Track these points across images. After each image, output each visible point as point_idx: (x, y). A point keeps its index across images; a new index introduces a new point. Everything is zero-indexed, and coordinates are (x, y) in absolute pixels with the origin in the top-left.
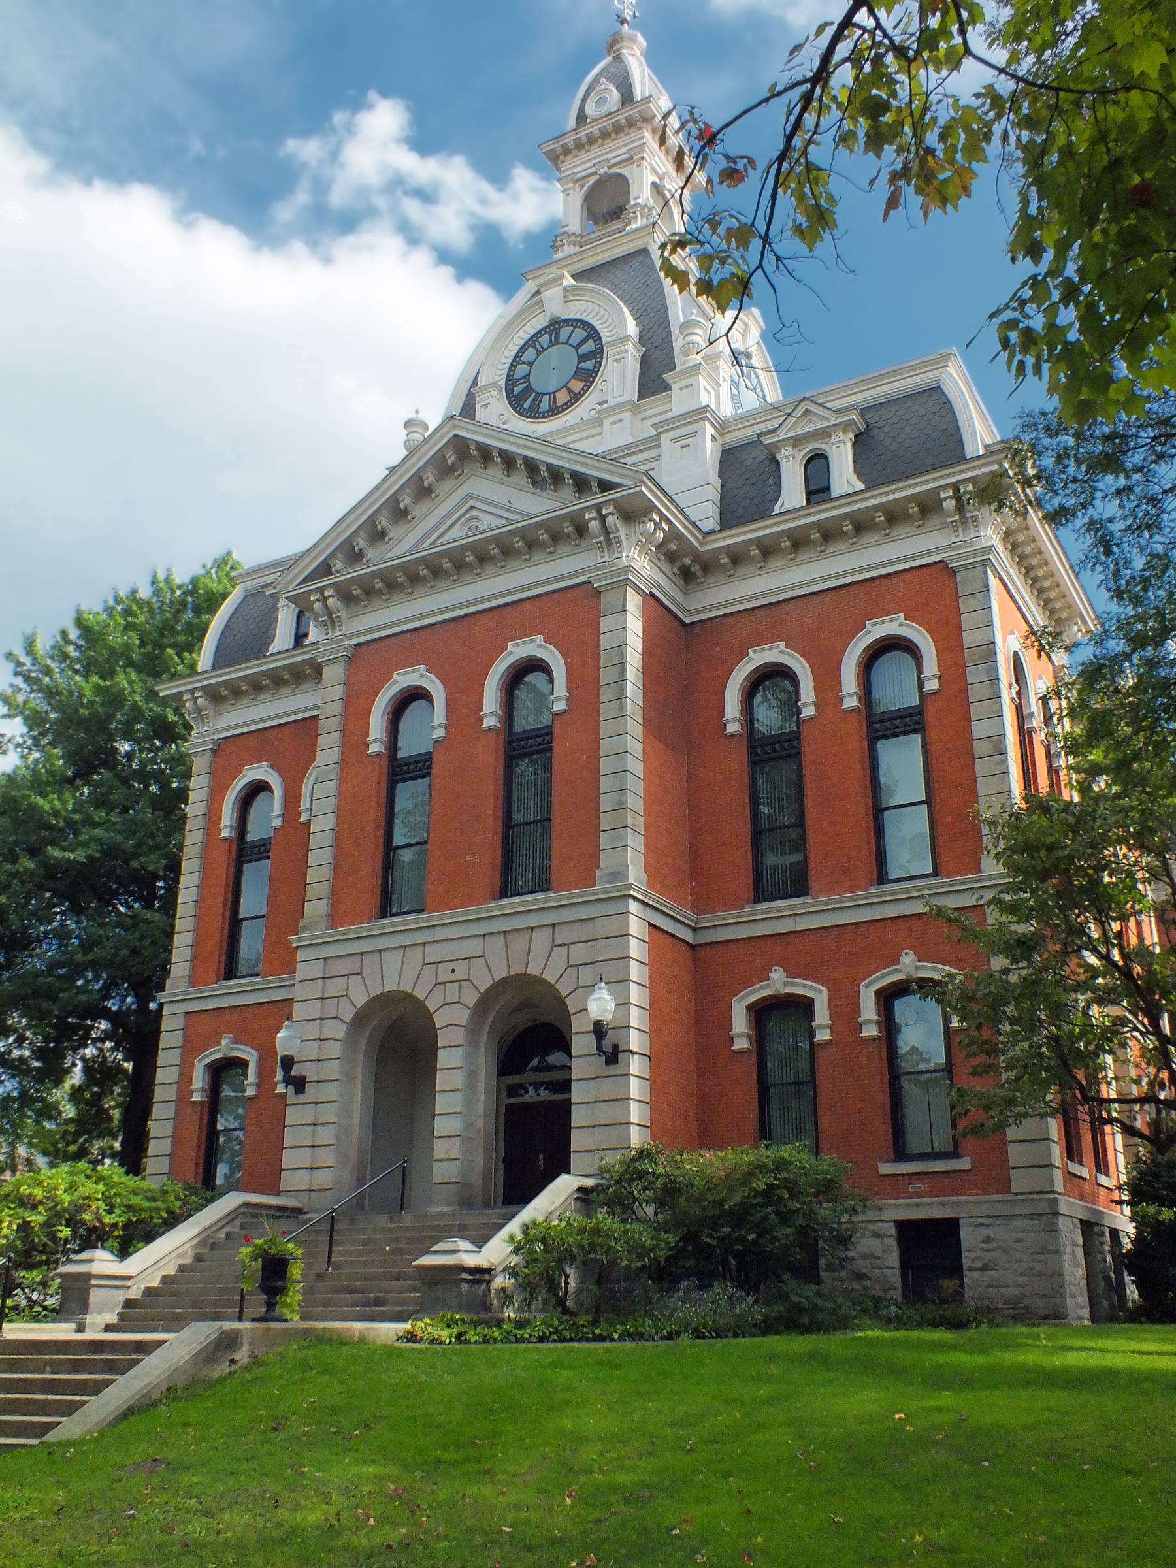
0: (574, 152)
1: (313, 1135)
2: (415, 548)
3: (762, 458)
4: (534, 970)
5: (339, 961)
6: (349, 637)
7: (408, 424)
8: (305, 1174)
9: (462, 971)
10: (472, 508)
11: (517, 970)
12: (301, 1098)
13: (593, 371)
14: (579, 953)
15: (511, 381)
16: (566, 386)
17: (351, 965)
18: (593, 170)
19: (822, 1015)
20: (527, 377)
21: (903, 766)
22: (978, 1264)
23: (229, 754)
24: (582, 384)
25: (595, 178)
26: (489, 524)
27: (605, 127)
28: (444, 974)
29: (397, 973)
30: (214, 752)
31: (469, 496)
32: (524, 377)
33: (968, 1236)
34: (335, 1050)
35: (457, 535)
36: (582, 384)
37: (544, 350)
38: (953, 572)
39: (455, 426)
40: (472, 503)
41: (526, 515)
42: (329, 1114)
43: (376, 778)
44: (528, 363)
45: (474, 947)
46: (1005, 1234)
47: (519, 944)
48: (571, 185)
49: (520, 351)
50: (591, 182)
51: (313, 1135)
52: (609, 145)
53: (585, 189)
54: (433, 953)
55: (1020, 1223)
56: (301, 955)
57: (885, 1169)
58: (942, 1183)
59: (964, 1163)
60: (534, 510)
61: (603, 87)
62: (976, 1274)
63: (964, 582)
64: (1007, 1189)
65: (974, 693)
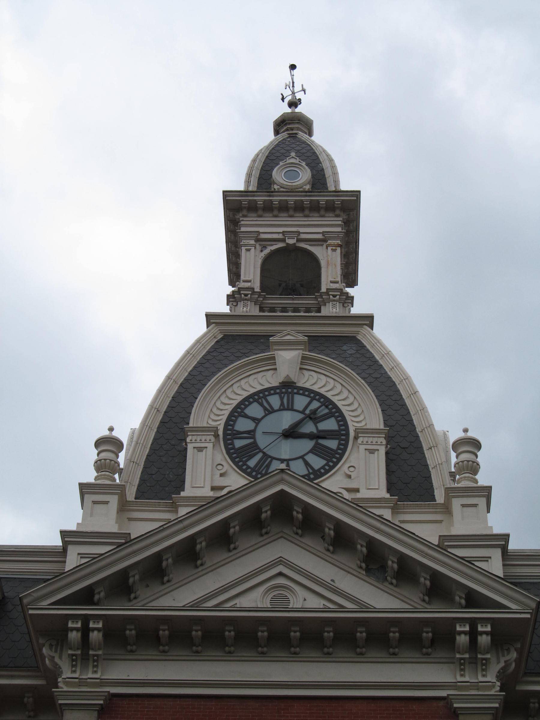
0: (260, 212)
2: (196, 605)
7: (99, 443)
10: (281, 574)
13: (335, 451)
15: (230, 434)
16: (302, 457)
18: (280, 236)
20: (251, 433)
24: (324, 462)
25: (280, 245)
26: (304, 602)
27: (318, 201)
32: (249, 432)
35: (255, 602)
36: (324, 462)
37: (274, 411)
39: (282, 481)
41: (364, 607)
44: (253, 419)
48: (252, 242)
49: (242, 402)
50: (273, 248)
52: (268, 219)
53: (267, 251)
60: (379, 605)
61: (292, 161)
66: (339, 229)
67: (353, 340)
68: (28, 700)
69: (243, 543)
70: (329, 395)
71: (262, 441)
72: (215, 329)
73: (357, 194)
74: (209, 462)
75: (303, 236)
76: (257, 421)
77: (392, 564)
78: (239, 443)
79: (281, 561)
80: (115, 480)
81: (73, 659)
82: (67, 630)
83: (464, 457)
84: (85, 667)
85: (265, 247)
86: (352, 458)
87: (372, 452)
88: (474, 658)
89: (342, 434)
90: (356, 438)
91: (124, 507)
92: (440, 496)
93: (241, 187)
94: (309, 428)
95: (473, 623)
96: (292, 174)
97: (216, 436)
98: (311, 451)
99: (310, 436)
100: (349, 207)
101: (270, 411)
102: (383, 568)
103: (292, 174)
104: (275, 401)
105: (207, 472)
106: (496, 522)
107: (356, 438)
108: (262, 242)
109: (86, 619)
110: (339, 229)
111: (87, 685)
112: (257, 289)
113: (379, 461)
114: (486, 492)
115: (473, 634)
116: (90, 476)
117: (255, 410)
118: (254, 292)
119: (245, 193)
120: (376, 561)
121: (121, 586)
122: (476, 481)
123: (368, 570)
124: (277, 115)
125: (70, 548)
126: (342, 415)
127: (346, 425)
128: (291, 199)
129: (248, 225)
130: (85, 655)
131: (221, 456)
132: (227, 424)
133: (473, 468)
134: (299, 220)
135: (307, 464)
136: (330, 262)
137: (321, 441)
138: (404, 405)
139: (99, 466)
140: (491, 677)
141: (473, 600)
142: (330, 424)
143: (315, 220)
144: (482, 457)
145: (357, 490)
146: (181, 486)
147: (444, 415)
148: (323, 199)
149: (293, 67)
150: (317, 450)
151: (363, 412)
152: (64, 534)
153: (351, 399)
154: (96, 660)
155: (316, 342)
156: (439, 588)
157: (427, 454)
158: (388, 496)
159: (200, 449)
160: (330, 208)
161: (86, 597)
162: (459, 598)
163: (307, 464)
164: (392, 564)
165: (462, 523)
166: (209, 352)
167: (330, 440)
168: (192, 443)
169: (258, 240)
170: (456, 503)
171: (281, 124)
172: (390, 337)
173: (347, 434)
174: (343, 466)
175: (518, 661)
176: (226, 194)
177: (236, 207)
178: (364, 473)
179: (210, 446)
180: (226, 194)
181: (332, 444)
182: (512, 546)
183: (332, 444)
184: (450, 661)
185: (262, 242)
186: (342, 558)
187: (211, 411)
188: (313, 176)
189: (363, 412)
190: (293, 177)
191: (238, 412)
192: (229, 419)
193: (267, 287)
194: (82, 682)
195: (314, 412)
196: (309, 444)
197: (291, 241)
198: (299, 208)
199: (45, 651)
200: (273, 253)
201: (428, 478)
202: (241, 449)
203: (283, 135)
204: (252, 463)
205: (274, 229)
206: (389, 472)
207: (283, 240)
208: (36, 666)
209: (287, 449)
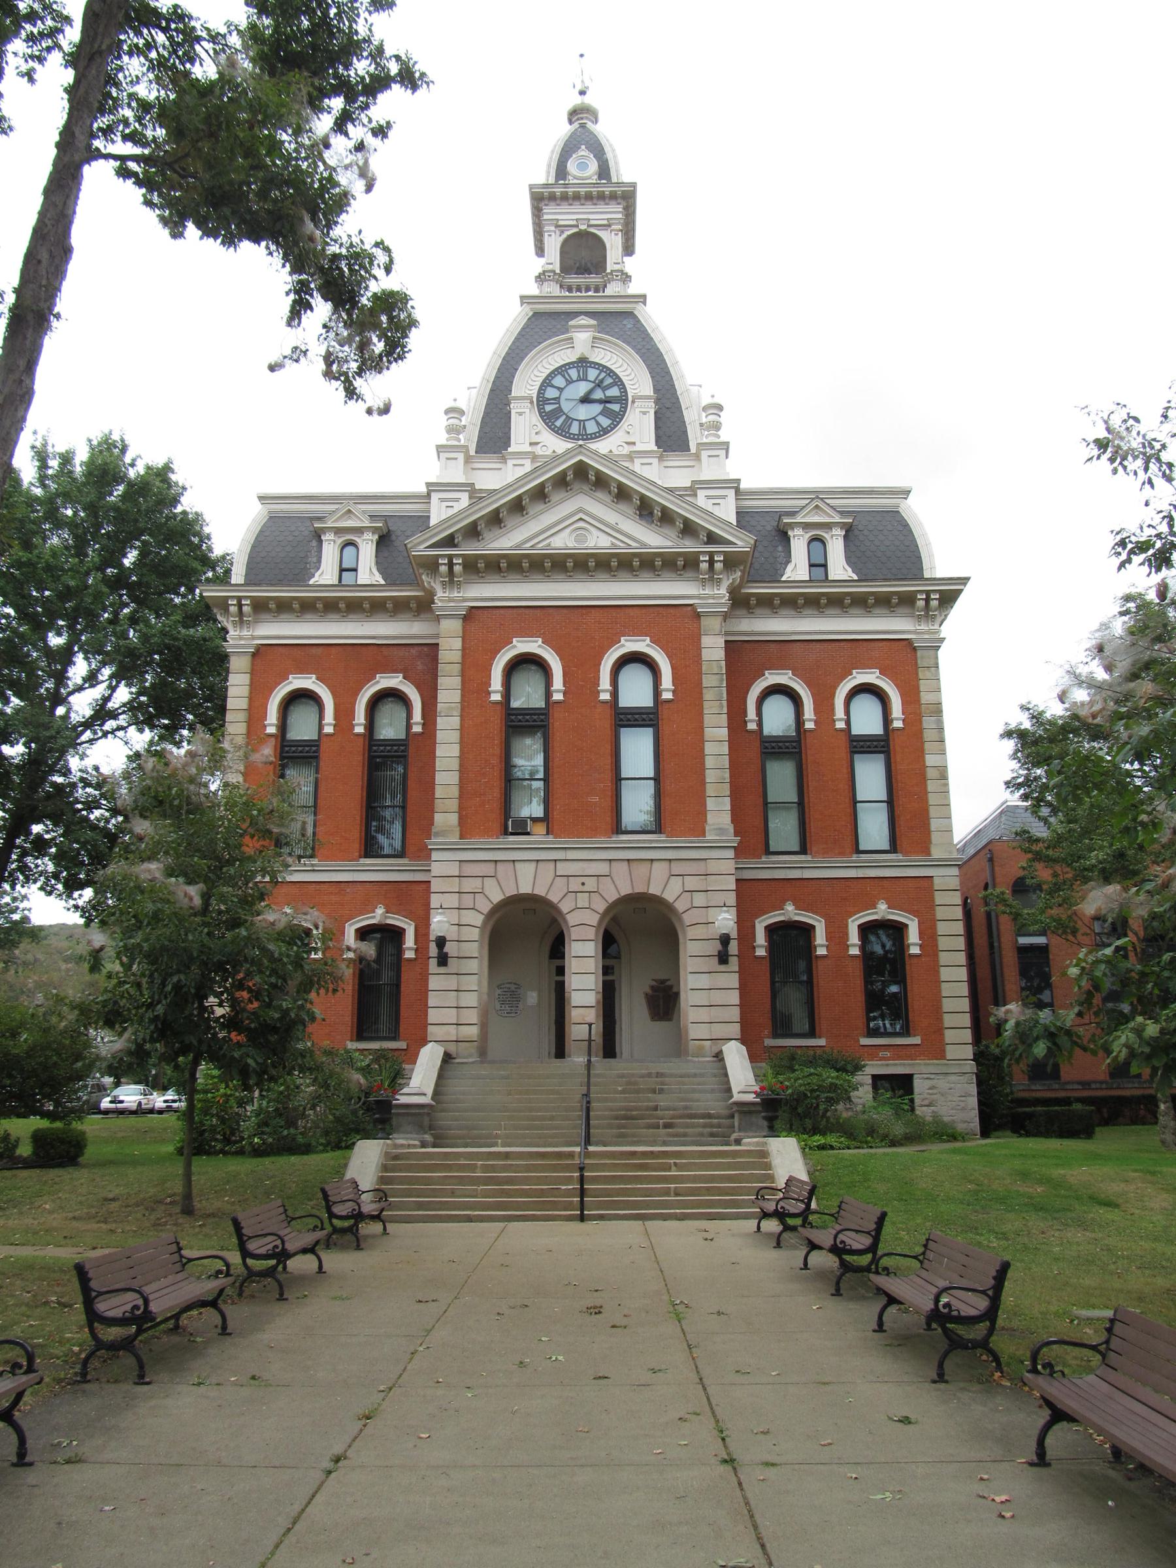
1: (458, 998)
3: (769, 528)
4: (654, 890)
5: (472, 865)
6: (465, 600)
7: (447, 412)
8: (452, 1029)
9: (591, 884)
11: (640, 889)
12: (442, 970)
14: (692, 883)
15: (542, 401)
17: (488, 869)
18: (574, 223)
19: (820, 938)
21: (870, 778)
22: (926, 1102)
23: (270, 661)
25: (575, 230)
26: (598, 542)
28: (575, 885)
29: (527, 879)
30: (254, 655)
31: (581, 510)
33: (918, 1084)
34: (475, 934)
38: (915, 649)
39: (580, 453)
40: (581, 515)
41: (645, 546)
42: (472, 983)
43: (496, 723)
44: (558, 388)
45: (603, 868)
46: (942, 1083)
47: (641, 870)
48: (553, 228)
49: (549, 375)
50: (569, 233)
51: (458, 998)
52: (565, 208)
53: (565, 236)
54: (563, 869)
55: (953, 1078)
56: (435, 856)
57: (865, 1041)
58: (901, 1052)
59: (916, 1040)
61: (583, 153)
62: (924, 1108)
63: (922, 658)
64: (943, 1057)
65: (928, 735)
66: (620, 216)
67: (630, 314)
68: (413, 605)
69: (555, 497)
70: (612, 367)
71: (566, 406)
72: (527, 308)
73: (634, 185)
74: (527, 423)
75: (592, 222)
76: (561, 390)
77: (657, 513)
78: (548, 408)
79: (581, 510)
80: (459, 440)
81: (443, 584)
82: (437, 565)
83: (711, 418)
84: (452, 589)
85: (562, 232)
86: (631, 417)
87: (644, 413)
88: (712, 578)
89: (623, 400)
90: (633, 402)
91: (468, 460)
92: (693, 449)
93: (543, 181)
94: (598, 394)
95: (711, 554)
96: (583, 166)
97: (532, 402)
98: (600, 414)
99: (600, 401)
100: (627, 197)
101: (570, 382)
102: (651, 514)
103: (583, 166)
104: (573, 373)
105: (525, 427)
106: (732, 468)
107: (633, 402)
108: (560, 228)
109: (450, 557)
110: (620, 216)
111: (453, 601)
112: (558, 271)
113: (650, 421)
114: (725, 446)
115: (711, 562)
116: (443, 438)
117: (559, 381)
118: (555, 273)
119: (546, 186)
120: (646, 510)
121: (473, 531)
122: (719, 437)
123: (641, 515)
124: (570, 106)
125: (433, 494)
126: (623, 384)
127: (626, 392)
128: (583, 190)
129: (550, 212)
130: (451, 580)
131: (536, 419)
132: (539, 393)
133: (717, 426)
134: (589, 208)
135: (598, 423)
136: (613, 242)
137: (608, 405)
138: (668, 373)
139: (451, 430)
140: (723, 591)
141: (712, 538)
142: (614, 392)
143: (601, 207)
144: (724, 417)
145: (634, 443)
146: (507, 443)
147: (696, 379)
148: (607, 190)
149: (582, 56)
150: (606, 413)
151: (638, 381)
152: (428, 484)
153: (629, 371)
154: (459, 584)
155: (602, 317)
156: (689, 529)
157: (685, 413)
158: (656, 448)
159: (520, 414)
160: (613, 197)
161: (450, 541)
162: (703, 536)
163: (598, 423)
164: (657, 513)
165: (708, 470)
166: (523, 329)
167: (613, 405)
168: (515, 408)
169: (557, 226)
170: (704, 454)
171: (575, 114)
172: (658, 317)
173: (627, 400)
174: (624, 425)
175: (742, 578)
176: (531, 187)
177: (540, 199)
178: (639, 426)
179: (527, 411)
180: (531, 187)
181: (616, 407)
182: (743, 486)
183: (616, 407)
184: (696, 580)
185: (560, 228)
186: (623, 506)
187: (526, 383)
188: (599, 166)
189: (638, 381)
190: (583, 170)
191: (547, 383)
192: (540, 389)
193: (565, 269)
194: (451, 600)
195: (602, 381)
196: (598, 408)
197: (583, 227)
198: (589, 197)
199: (423, 577)
200: (570, 237)
201: (685, 432)
202: (551, 415)
203: (576, 125)
204: (558, 423)
205: (570, 216)
206: (657, 428)
207: (577, 226)
208: (418, 584)
209: (583, 412)
